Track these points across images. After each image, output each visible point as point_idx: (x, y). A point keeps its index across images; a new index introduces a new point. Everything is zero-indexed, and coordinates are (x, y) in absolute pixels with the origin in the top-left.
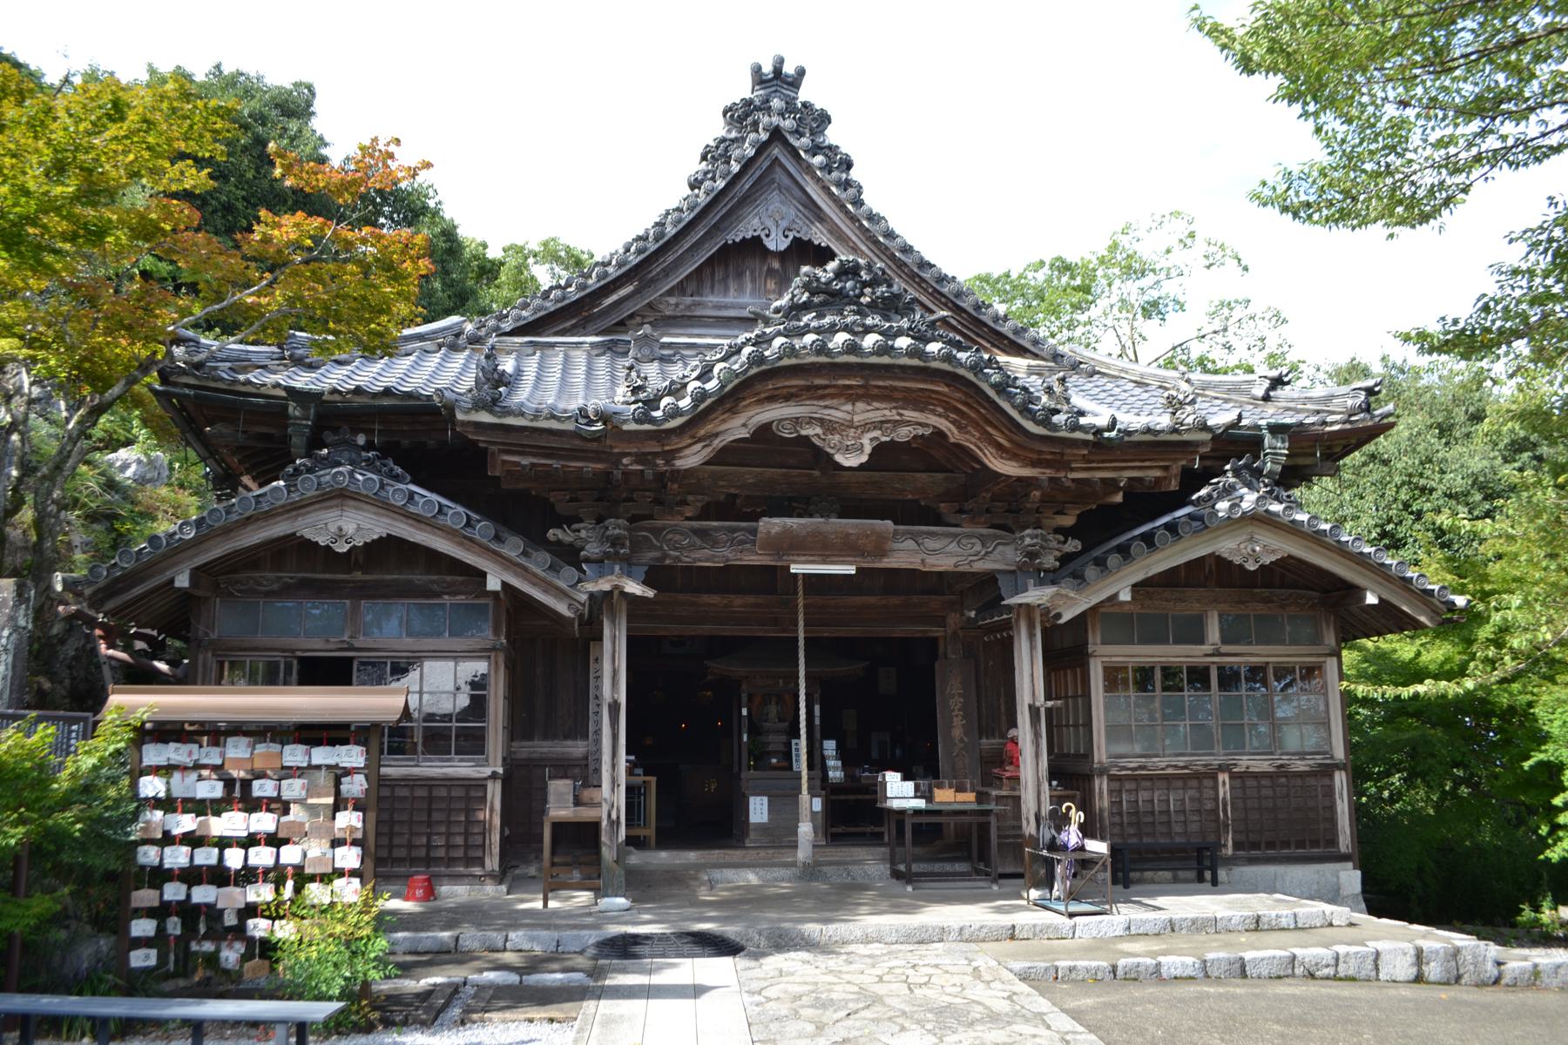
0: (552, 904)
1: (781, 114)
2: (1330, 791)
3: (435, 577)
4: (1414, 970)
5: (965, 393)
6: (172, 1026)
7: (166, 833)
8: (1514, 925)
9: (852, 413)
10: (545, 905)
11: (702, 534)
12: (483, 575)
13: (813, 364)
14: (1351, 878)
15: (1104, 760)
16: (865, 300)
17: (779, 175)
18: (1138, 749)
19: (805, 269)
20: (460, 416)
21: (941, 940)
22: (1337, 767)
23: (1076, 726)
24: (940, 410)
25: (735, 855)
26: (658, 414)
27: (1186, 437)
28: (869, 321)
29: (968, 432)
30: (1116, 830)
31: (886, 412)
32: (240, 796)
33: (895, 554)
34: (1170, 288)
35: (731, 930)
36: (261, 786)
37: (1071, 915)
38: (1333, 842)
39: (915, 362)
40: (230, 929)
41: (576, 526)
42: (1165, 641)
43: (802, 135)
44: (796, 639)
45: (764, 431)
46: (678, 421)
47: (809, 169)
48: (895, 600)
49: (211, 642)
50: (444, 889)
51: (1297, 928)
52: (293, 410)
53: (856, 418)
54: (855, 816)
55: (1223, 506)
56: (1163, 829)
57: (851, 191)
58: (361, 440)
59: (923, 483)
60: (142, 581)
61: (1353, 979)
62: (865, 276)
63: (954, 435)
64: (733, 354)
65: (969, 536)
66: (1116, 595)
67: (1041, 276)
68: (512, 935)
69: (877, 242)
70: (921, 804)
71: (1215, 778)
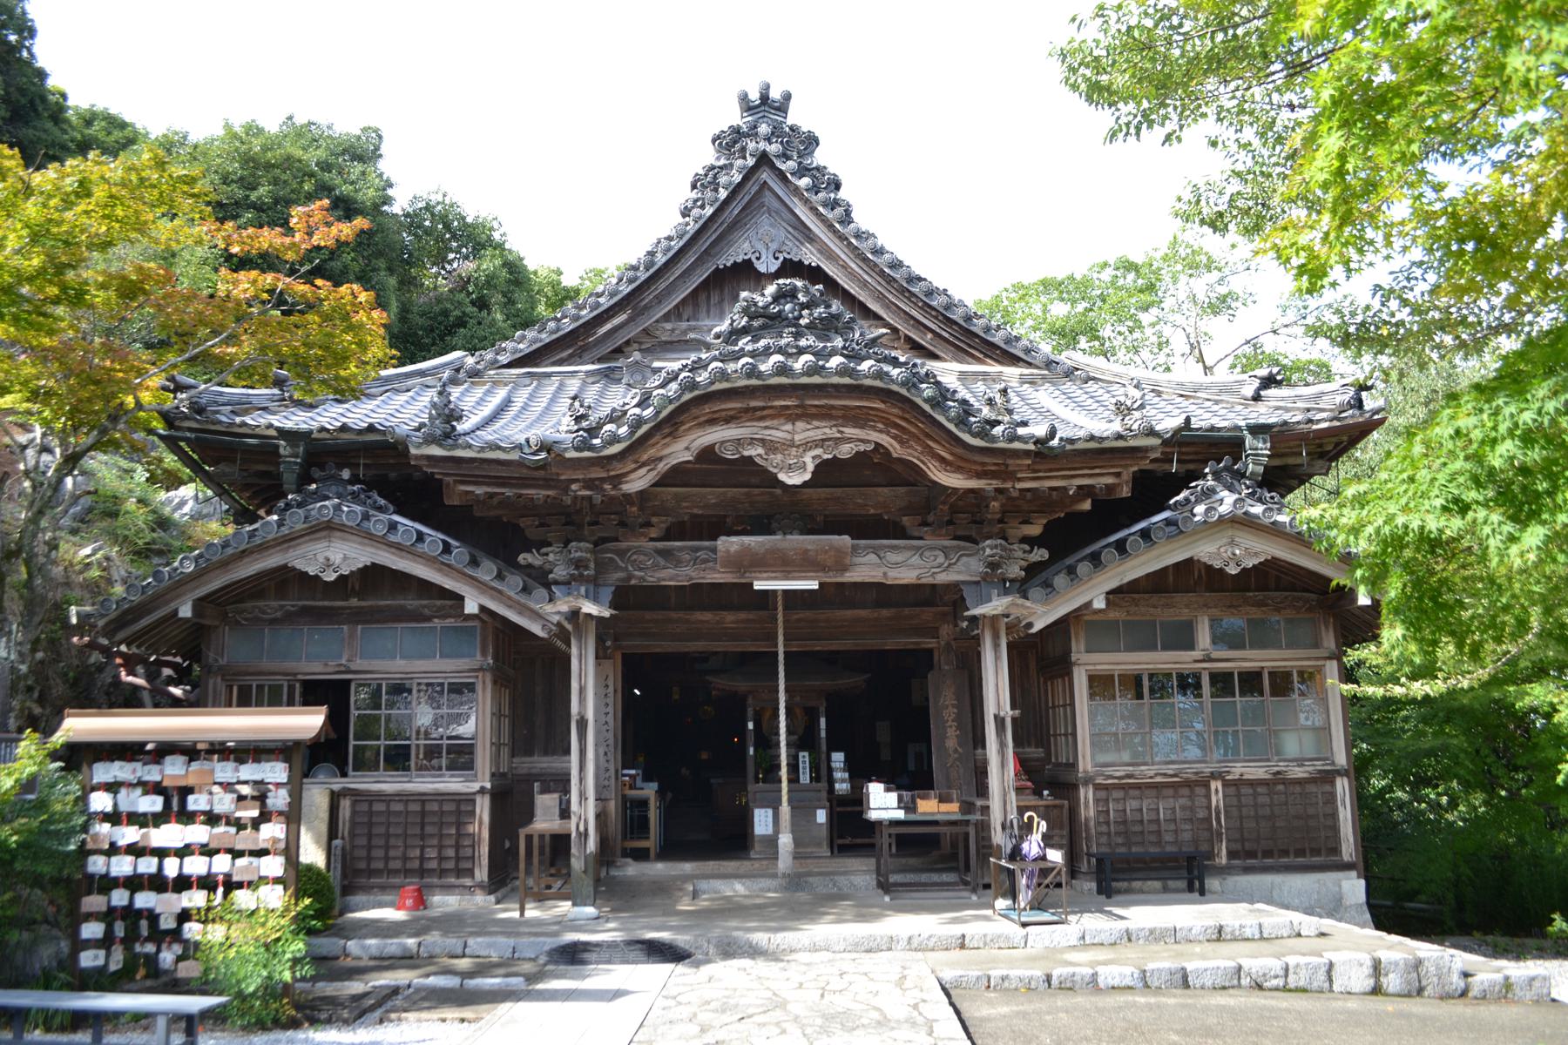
0: (529, 914)
1: (768, 140)
2: (1331, 799)
3: (425, 602)
4: (1371, 982)
5: (903, 410)
6: (122, 1020)
7: (112, 844)
8: (1544, 936)
9: (793, 433)
10: (522, 914)
11: (666, 554)
12: (462, 598)
13: (747, 387)
14: (1354, 887)
15: (1089, 768)
16: (803, 322)
17: (768, 198)
18: (1126, 757)
19: (744, 294)
20: (413, 451)
21: (890, 949)
22: (1339, 773)
23: (1066, 735)
24: (880, 426)
25: (730, 866)
26: (596, 441)
27: (1132, 443)
28: (803, 343)
29: (910, 447)
30: (1104, 840)
31: (826, 430)
32: (176, 807)
33: (858, 569)
34: (1236, 284)
35: (681, 939)
36: (195, 801)
37: (1024, 925)
38: (1336, 850)
39: (847, 380)
40: (168, 932)
41: (544, 550)
42: (1153, 648)
43: (788, 158)
44: (776, 654)
45: (707, 454)
46: (616, 449)
47: (796, 191)
48: (885, 613)
49: (220, 668)
50: (437, 899)
51: (1262, 938)
52: (284, 448)
53: (797, 437)
54: (851, 831)
55: (1200, 509)
56: (1153, 838)
57: (839, 211)
58: (346, 474)
59: (882, 499)
60: (149, 612)
61: (1304, 990)
62: (802, 298)
63: (896, 450)
64: (671, 381)
65: (932, 548)
66: (1089, 603)
67: (1107, 275)
68: (471, 941)
69: (865, 260)
70: (900, 815)
71: (1207, 786)
